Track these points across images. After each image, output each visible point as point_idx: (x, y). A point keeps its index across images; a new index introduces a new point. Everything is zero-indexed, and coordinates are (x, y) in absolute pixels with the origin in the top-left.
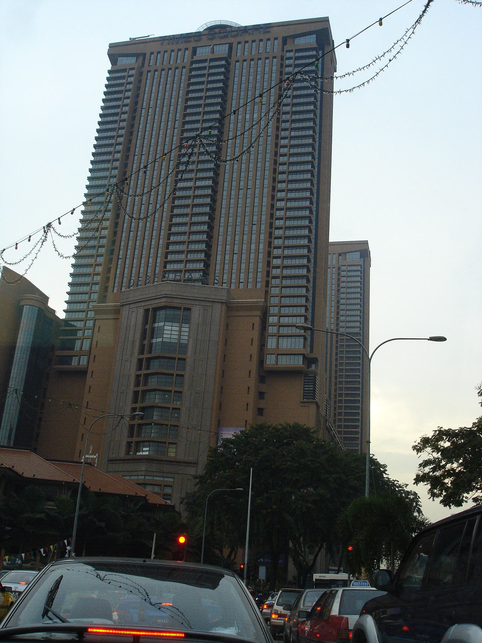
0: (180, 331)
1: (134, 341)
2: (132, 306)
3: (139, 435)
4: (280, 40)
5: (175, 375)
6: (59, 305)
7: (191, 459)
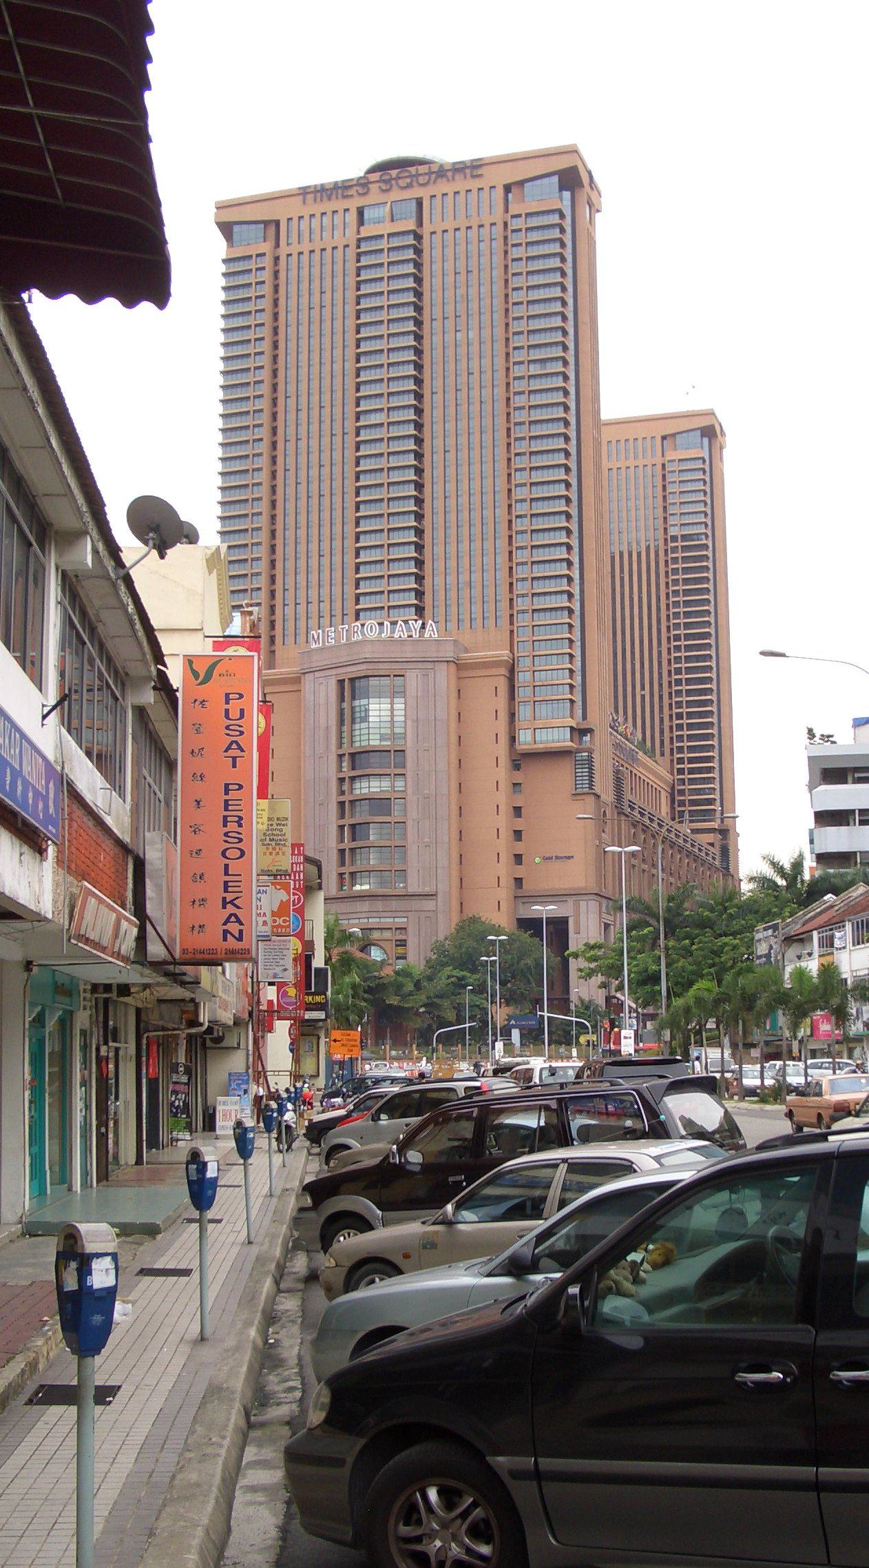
0: (392, 710)
3: (353, 863)
4: (500, 191)
7: (427, 890)
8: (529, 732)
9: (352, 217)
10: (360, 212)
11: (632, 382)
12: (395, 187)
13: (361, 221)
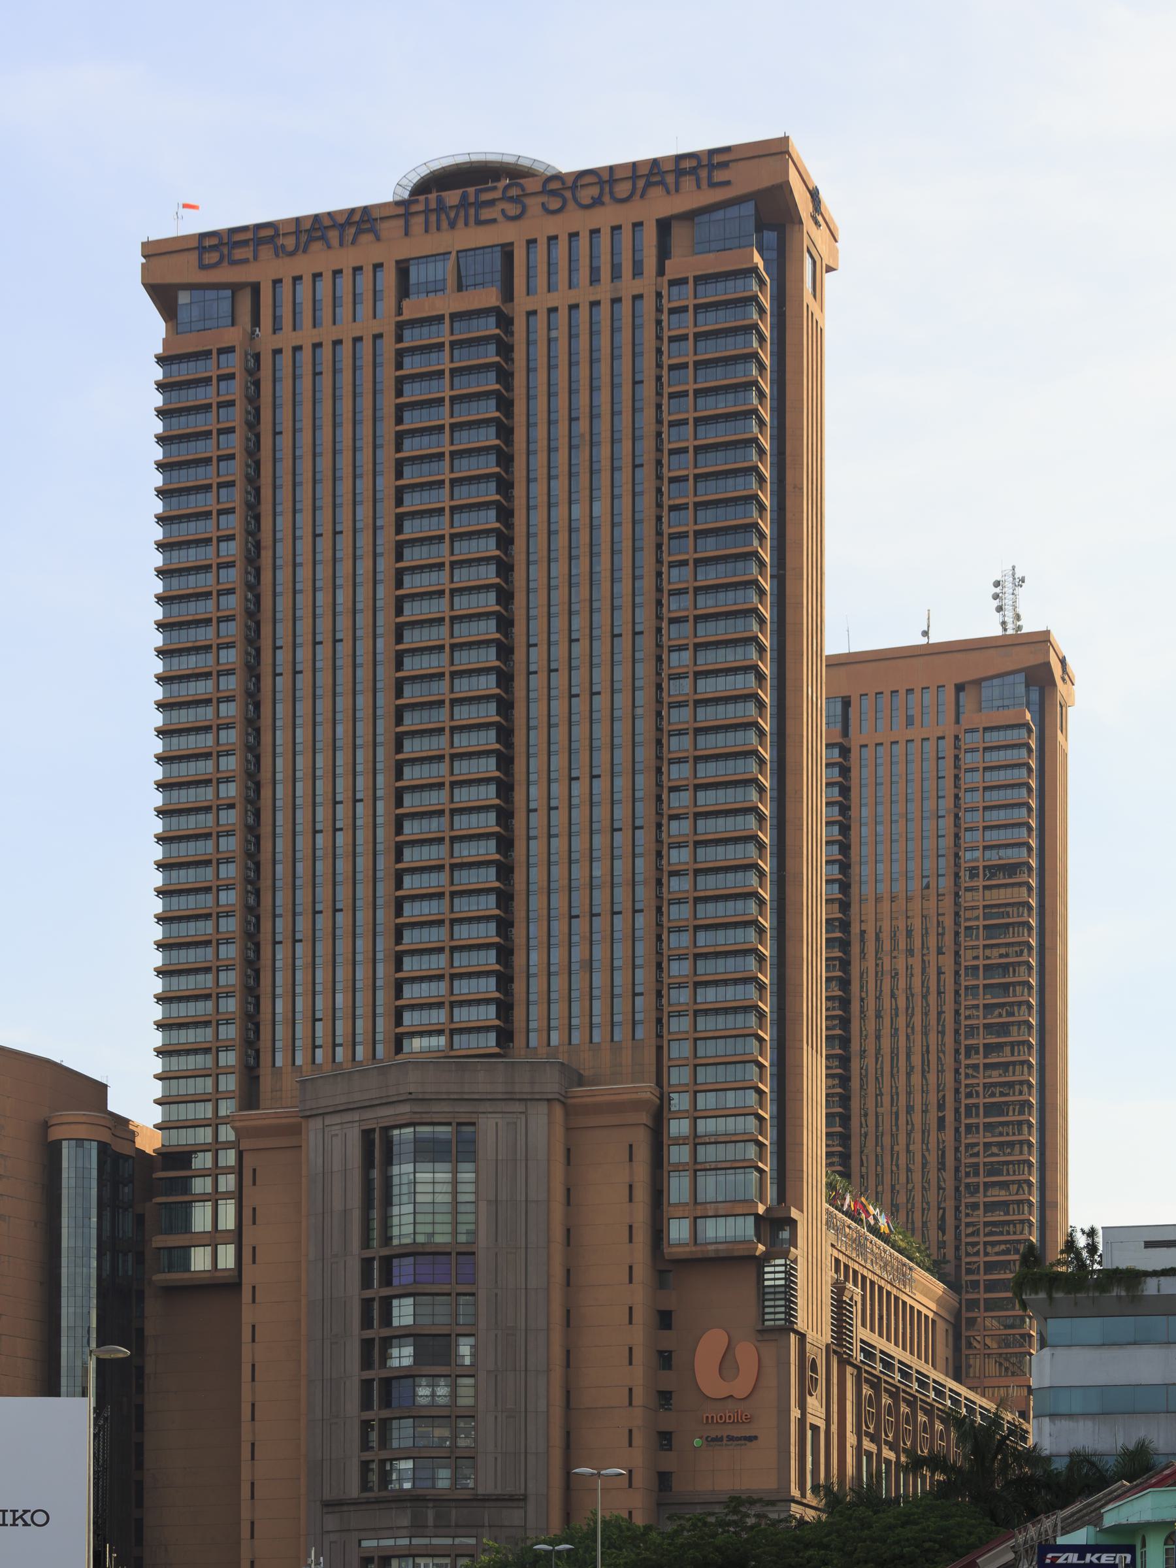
0: (455, 1182)
1: (345, 1212)
2: (329, 1120)
8: (686, 1224)
9: (388, 279)
10: (403, 269)
11: (884, 576)
12: (571, 205)
13: (404, 290)
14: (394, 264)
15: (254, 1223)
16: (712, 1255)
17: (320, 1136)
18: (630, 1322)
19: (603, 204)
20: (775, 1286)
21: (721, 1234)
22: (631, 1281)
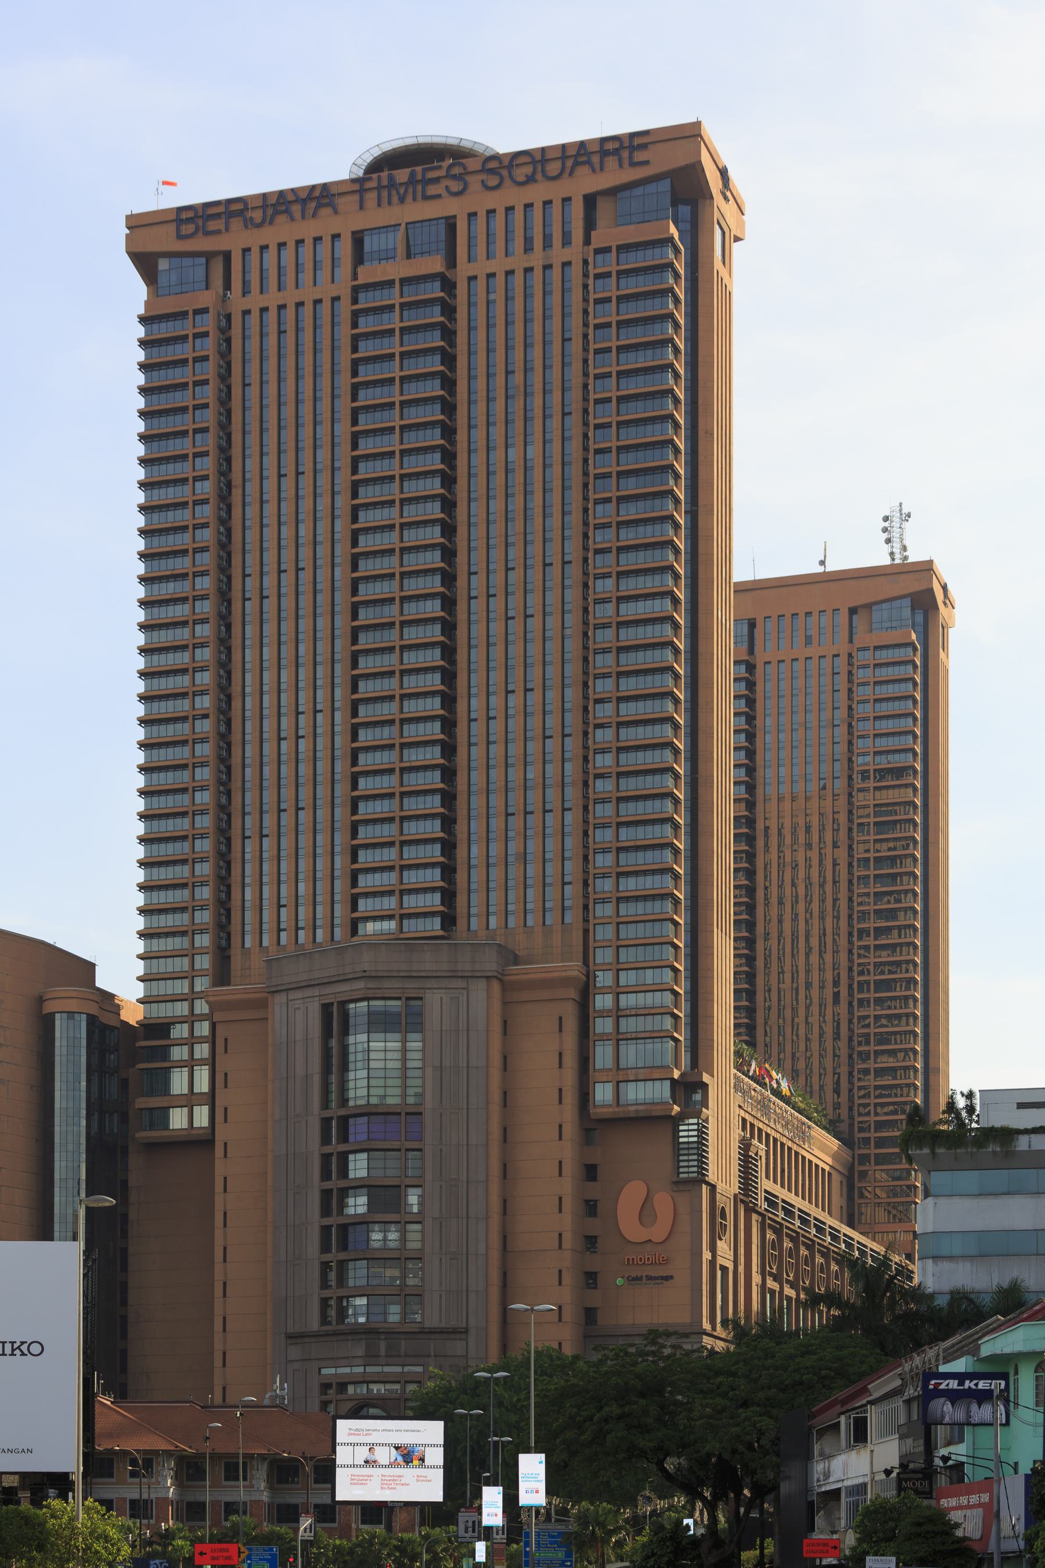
0: (404, 1050)
1: (307, 1077)
2: (292, 995)
5: (403, 1114)
6: (122, 976)
8: (609, 1088)
9: (345, 248)
10: (358, 239)
12: (508, 182)
13: (359, 258)
14: (350, 234)
15: (226, 1087)
16: (633, 1115)
17: (284, 1009)
18: (560, 1175)
19: (536, 181)
20: (688, 1143)
21: (641, 1096)
22: (560, 1138)
